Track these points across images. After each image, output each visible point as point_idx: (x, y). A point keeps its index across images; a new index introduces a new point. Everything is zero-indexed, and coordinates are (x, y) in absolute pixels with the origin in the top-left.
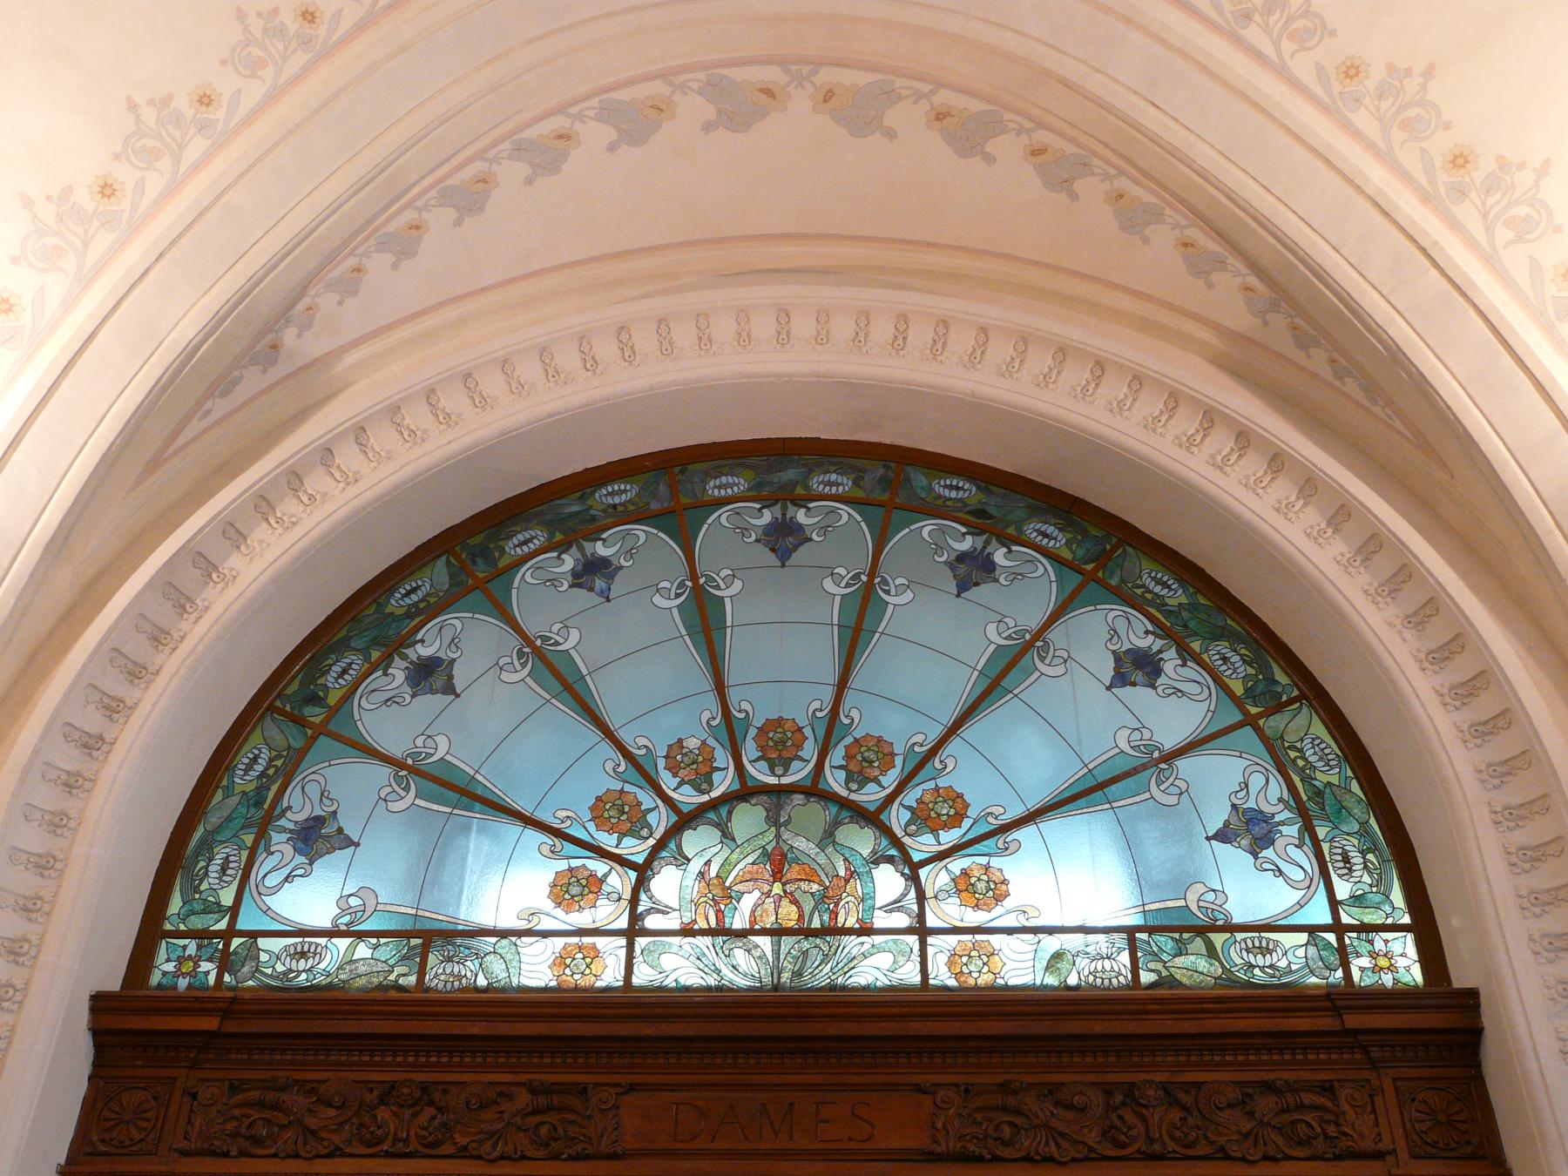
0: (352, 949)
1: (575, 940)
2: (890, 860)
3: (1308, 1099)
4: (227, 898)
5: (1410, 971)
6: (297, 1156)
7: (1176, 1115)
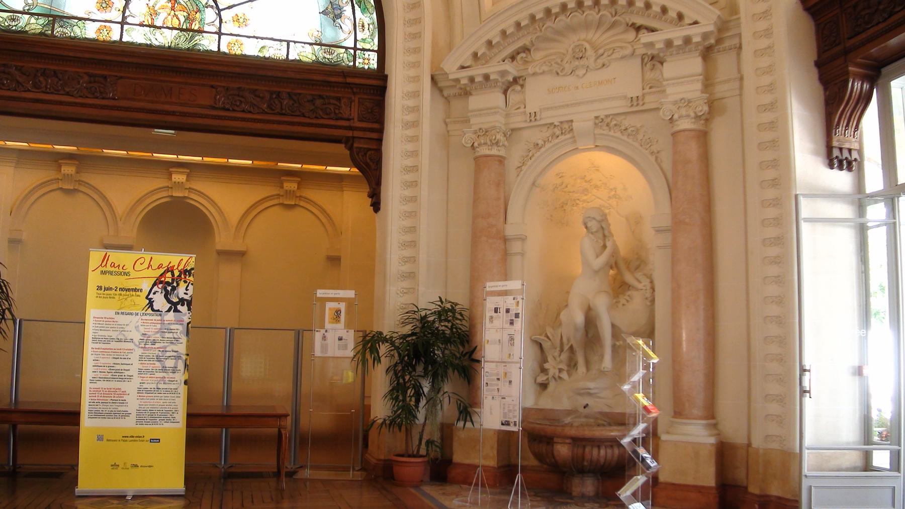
0: (29, 19)
1: (103, 24)
2: (212, 7)
3: (332, 101)
5: (374, 65)
6: (16, 90)
7: (291, 102)
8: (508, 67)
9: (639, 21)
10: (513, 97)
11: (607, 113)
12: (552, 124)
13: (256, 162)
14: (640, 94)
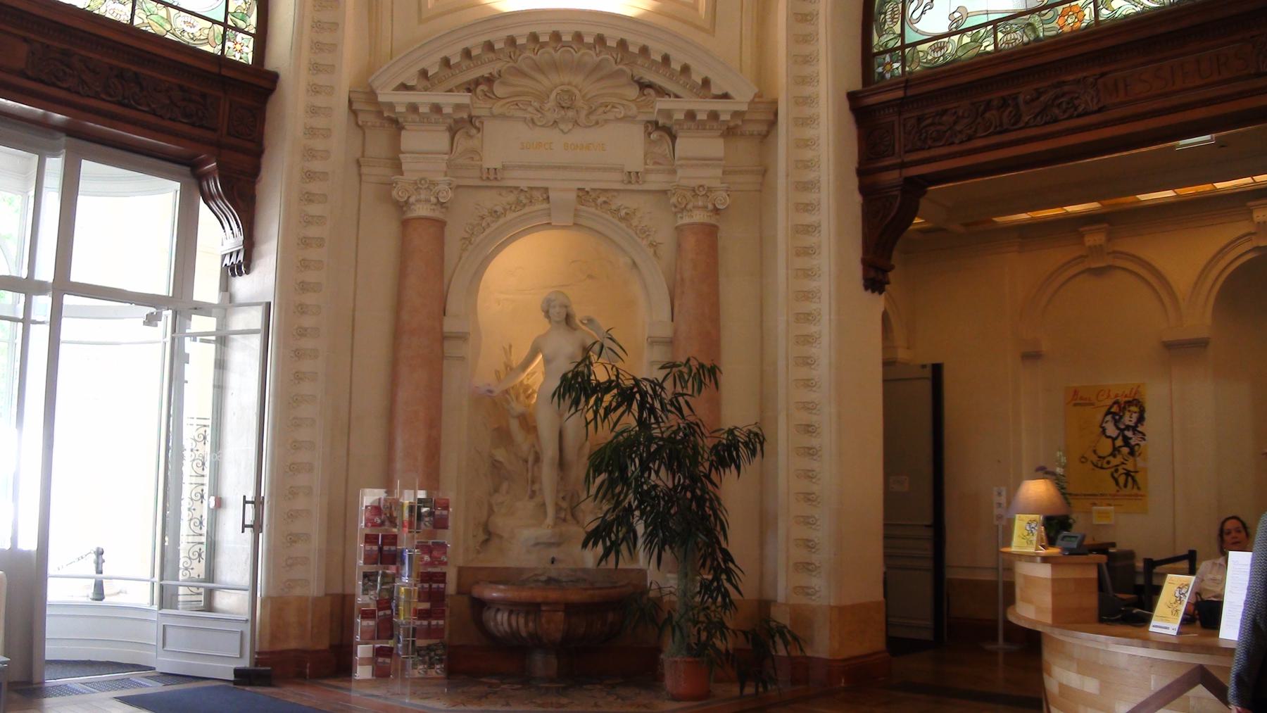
4: (897, 29)
8: (464, 98)
9: (649, 77)
10: (462, 143)
11: (596, 186)
12: (516, 188)
13: (1107, 202)
14: (641, 169)
